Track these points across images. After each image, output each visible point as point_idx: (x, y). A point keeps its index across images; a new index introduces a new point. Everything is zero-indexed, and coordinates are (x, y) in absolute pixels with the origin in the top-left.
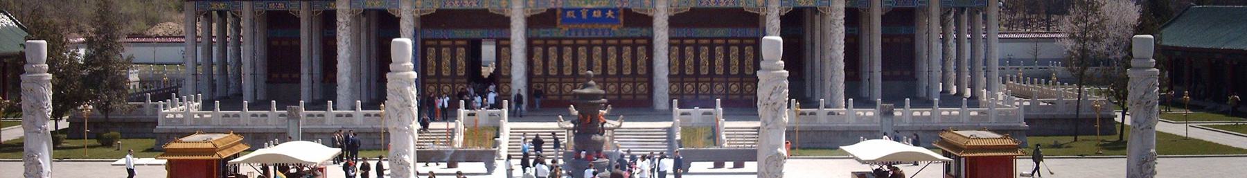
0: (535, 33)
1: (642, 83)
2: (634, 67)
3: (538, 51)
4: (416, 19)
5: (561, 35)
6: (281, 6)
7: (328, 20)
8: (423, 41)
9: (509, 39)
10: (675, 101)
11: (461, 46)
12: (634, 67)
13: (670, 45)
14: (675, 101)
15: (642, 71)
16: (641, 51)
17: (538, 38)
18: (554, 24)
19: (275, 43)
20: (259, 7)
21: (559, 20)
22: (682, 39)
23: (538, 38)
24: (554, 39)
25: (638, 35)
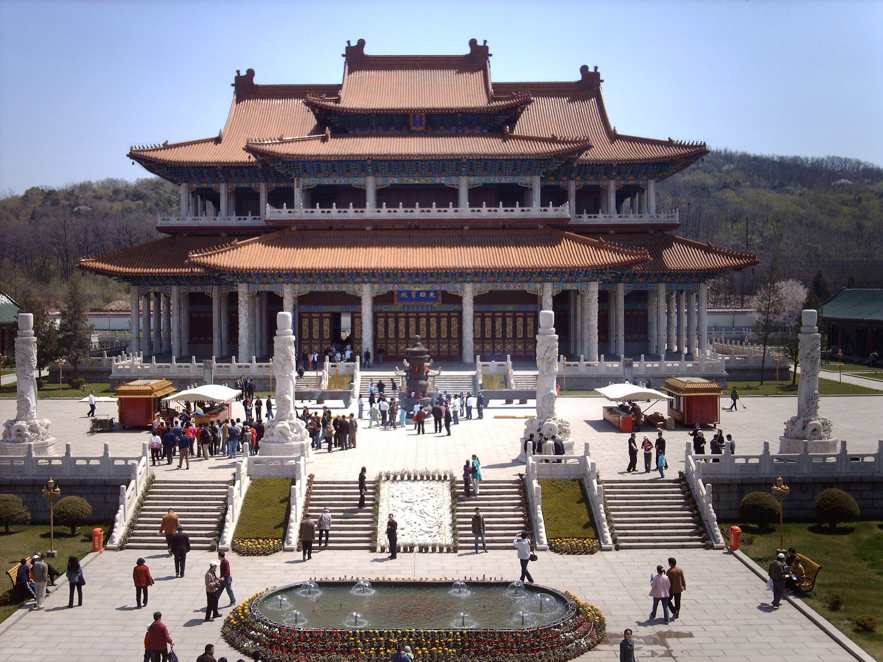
3: (381, 321)
4: (294, 298)
5: (397, 310)
6: (199, 289)
8: (300, 314)
9: (360, 313)
10: (478, 356)
11: (327, 317)
12: (449, 332)
13: (475, 317)
14: (478, 356)
15: (454, 335)
18: (392, 302)
20: (185, 289)
21: (396, 299)
22: (483, 312)
25: (452, 309)
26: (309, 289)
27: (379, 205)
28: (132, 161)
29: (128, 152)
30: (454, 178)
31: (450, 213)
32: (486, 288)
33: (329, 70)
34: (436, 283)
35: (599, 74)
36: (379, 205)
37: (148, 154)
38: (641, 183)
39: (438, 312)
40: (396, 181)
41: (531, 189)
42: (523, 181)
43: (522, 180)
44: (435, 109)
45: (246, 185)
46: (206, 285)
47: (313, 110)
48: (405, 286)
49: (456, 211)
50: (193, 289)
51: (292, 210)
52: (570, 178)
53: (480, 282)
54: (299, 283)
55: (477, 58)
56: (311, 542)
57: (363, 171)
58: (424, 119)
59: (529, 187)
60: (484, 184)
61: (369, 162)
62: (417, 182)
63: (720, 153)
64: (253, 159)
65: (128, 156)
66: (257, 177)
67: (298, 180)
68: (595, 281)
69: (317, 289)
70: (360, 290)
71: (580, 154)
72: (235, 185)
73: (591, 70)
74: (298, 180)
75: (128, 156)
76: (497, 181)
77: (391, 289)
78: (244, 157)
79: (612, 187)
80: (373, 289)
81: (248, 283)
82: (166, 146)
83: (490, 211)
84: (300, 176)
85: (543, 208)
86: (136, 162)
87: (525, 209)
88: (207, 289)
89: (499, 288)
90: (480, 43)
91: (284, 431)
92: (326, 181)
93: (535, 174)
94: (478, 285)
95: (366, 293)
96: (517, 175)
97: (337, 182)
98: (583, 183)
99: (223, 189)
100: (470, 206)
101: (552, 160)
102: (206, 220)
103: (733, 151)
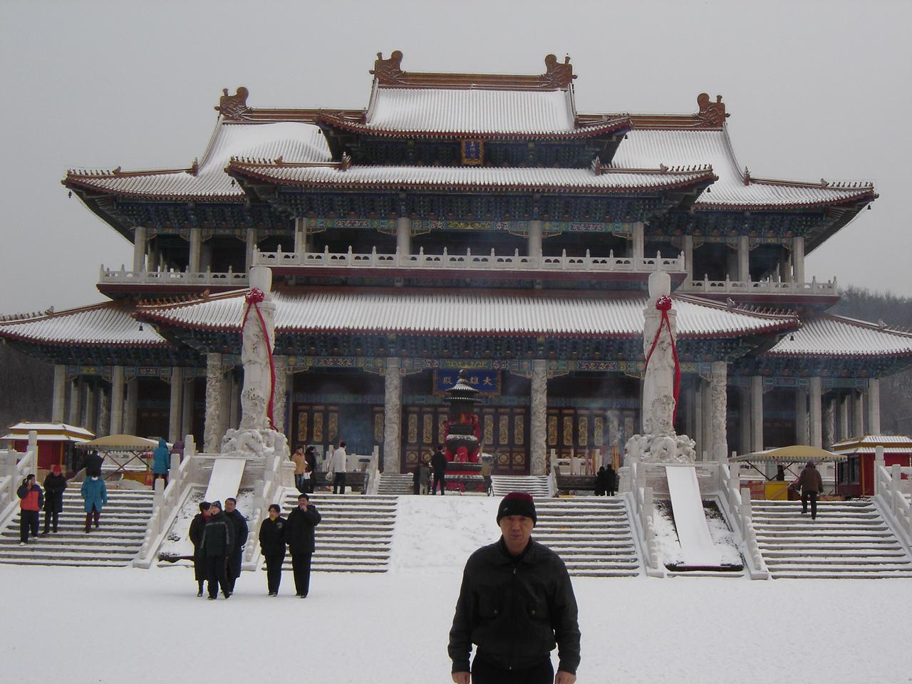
0: (410, 399)
1: (519, 453)
2: (511, 437)
3: (413, 419)
4: (288, 377)
5: (438, 401)
6: (152, 372)
7: (152, 499)
8: (295, 405)
9: (383, 406)
10: (553, 451)
11: (335, 411)
12: (511, 437)
13: (548, 415)
14: (553, 451)
15: (519, 441)
16: (519, 420)
17: (413, 405)
18: (430, 392)
19: (145, 415)
20: (131, 371)
21: (435, 386)
22: (561, 409)
23: (413, 405)
24: (428, 406)
25: (515, 403)
26: (310, 364)
27: (414, 251)
28: (68, 190)
29: (64, 177)
30: (522, 224)
31: (516, 264)
32: (566, 367)
33: (349, 91)
34: (494, 359)
35: (723, 105)
36: (414, 251)
37: (92, 182)
38: (784, 241)
39: (497, 407)
40: (440, 225)
41: (631, 242)
42: (620, 230)
43: (618, 228)
44: (497, 134)
45: (227, 232)
46: (163, 366)
47: (326, 134)
48: (448, 362)
49: (524, 261)
50: (143, 372)
51: (290, 254)
52: (684, 232)
53: (557, 359)
54: (295, 355)
55: (558, 75)
56: (282, 562)
57: (393, 210)
58: (481, 148)
59: (628, 238)
60: (565, 233)
61: (403, 195)
62: (469, 227)
63: (881, 299)
64: (237, 190)
65: (63, 182)
66: (243, 220)
67: (301, 220)
68: (722, 359)
69: (322, 364)
70: (384, 367)
71: (700, 192)
72: (211, 232)
73: (713, 100)
74: (301, 220)
75: (63, 182)
76: (583, 229)
77: (429, 366)
78: (230, 188)
79: (744, 246)
80: (401, 367)
81: (222, 352)
82: (118, 174)
83: (572, 261)
84: (304, 215)
85: (647, 260)
86: (74, 194)
87: (623, 259)
88: (163, 373)
89: (584, 368)
90: (561, 60)
91: (252, 442)
92: (340, 224)
93: (636, 220)
94: (554, 363)
95: (393, 375)
96: (611, 221)
97: (357, 225)
98: (703, 240)
99: (194, 237)
100: (544, 255)
101: (660, 199)
102: (171, 277)
103: (898, 296)
